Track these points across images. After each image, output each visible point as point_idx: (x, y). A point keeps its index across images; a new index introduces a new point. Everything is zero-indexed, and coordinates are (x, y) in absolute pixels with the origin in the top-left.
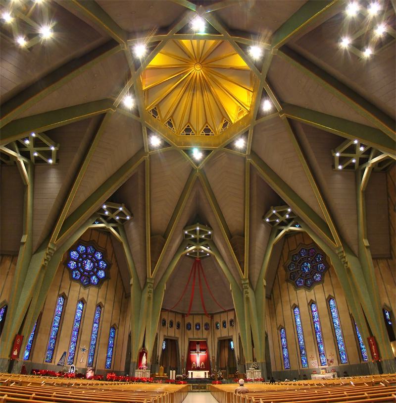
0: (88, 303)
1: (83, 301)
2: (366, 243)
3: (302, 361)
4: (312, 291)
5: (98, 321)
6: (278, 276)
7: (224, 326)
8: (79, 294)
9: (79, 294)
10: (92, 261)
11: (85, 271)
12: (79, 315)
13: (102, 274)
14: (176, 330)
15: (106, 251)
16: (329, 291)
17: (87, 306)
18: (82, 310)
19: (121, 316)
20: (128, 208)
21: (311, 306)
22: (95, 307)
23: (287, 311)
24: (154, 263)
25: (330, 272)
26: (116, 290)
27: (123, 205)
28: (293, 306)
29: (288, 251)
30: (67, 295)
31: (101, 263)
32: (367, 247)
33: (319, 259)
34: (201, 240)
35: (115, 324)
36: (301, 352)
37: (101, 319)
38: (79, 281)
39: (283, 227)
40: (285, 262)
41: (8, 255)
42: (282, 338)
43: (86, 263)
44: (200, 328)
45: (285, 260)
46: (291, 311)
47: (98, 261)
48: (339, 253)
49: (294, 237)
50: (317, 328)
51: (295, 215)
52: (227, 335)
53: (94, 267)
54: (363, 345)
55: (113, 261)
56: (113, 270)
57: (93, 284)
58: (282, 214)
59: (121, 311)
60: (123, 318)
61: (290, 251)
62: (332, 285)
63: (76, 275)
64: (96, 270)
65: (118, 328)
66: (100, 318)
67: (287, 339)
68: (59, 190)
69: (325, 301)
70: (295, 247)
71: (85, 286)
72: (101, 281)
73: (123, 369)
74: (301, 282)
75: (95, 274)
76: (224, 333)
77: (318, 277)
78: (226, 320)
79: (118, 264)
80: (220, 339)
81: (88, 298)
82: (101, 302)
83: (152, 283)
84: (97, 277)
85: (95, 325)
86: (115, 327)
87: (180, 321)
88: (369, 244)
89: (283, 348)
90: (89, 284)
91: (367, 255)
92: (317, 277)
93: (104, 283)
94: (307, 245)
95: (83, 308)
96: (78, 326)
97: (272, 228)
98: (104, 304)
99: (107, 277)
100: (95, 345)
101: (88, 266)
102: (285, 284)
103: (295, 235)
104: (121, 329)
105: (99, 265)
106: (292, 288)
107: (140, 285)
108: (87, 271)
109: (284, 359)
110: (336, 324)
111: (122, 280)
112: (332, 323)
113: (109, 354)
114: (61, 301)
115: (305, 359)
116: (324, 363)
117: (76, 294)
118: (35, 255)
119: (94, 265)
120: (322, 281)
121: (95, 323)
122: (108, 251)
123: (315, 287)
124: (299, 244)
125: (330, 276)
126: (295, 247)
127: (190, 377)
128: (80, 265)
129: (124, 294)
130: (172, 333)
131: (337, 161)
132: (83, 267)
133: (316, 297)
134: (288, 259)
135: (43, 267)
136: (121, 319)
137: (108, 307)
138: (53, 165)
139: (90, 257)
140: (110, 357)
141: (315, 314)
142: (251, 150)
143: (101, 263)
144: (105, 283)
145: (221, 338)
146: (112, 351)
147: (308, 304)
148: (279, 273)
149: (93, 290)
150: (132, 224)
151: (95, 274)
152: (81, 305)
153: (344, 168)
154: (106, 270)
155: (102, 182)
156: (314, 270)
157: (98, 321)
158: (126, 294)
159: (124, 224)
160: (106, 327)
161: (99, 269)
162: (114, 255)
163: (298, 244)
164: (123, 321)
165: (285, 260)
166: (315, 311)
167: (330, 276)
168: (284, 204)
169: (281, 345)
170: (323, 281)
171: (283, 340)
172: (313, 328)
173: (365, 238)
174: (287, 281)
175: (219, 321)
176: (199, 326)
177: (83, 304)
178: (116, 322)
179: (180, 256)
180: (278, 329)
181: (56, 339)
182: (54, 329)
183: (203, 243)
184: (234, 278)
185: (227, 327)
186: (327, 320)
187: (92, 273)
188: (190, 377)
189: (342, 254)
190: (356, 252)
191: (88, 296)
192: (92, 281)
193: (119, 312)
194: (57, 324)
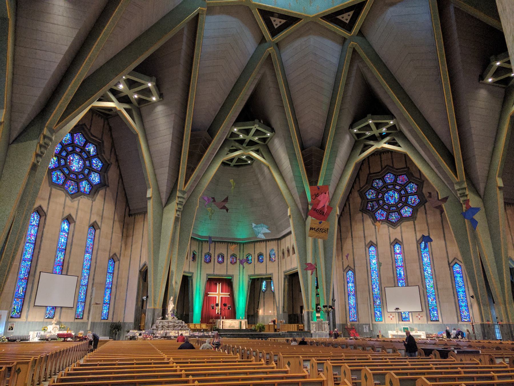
0: (76, 223)
1: (69, 219)
2: (500, 183)
3: (375, 313)
4: (399, 228)
5: (91, 250)
6: (349, 204)
7: (260, 261)
8: (64, 208)
9: (64, 208)
10: (82, 158)
11: (71, 172)
12: (63, 240)
13: (95, 178)
14: (191, 262)
15: (103, 142)
16: (422, 230)
17: (77, 226)
18: (68, 234)
19: (123, 242)
20: (158, 86)
21: (394, 246)
22: (88, 227)
23: (360, 247)
24: (190, 170)
25: (427, 207)
26: (116, 204)
27: (154, 78)
28: (368, 244)
29: (368, 172)
30: (45, 211)
31: (94, 162)
32: (500, 188)
33: (412, 189)
34: (251, 143)
35: (115, 254)
36: (374, 302)
37: (96, 246)
38: (62, 187)
39: (371, 143)
40: (361, 187)
41: (88, 181)
42: (348, 283)
43: (73, 160)
44: (223, 261)
45: (362, 184)
46: (366, 250)
47: (89, 158)
48: (459, 190)
49: (379, 156)
50: (400, 274)
51: (396, 129)
52: (265, 273)
53: (85, 167)
54: (463, 302)
55: (113, 160)
56: (113, 174)
57: (84, 194)
58: (378, 126)
59: (122, 235)
60: (126, 245)
61: (370, 174)
62: (428, 224)
63: (58, 178)
64: (86, 171)
65: (119, 260)
66: (93, 245)
67: (357, 283)
68: (71, 40)
69: (415, 242)
70: (379, 169)
71: (73, 196)
72: (94, 189)
73: (130, 318)
74: (382, 215)
75: (86, 178)
76: (260, 270)
77: (407, 212)
78: (264, 252)
79: (119, 166)
80: (252, 278)
81: (77, 214)
82: (95, 222)
83: (184, 198)
84: (90, 183)
85: (87, 256)
86: (115, 258)
87: (197, 251)
88: (504, 185)
89: (349, 295)
90: (78, 193)
91: (500, 198)
92: (406, 211)
93: (100, 192)
94: (397, 169)
95: (69, 230)
96: (62, 258)
97: (356, 141)
98: (99, 224)
99: (103, 184)
100: (87, 285)
101: (76, 164)
102: (360, 215)
103: (380, 155)
104: (124, 262)
105: (91, 163)
106: (369, 222)
107: (161, 199)
108: (73, 172)
109: (350, 308)
110: (427, 273)
111: (124, 189)
112: (422, 270)
113: (107, 298)
114: (34, 219)
115: (379, 311)
116: (406, 318)
117: (60, 208)
118: (14, 145)
119: (84, 164)
120: (413, 217)
121: (87, 252)
122: (105, 144)
123: (402, 224)
124: (385, 167)
125: (426, 213)
126: (379, 169)
127: (221, 328)
128: (62, 162)
129: (127, 210)
130: (188, 267)
131: (493, 70)
132: (67, 166)
133: (403, 236)
134: (367, 183)
135: (177, 219)
136: (123, 246)
137: (106, 228)
138: (489, 84)
139: (78, 150)
140: (107, 303)
141: (399, 257)
142: (360, 31)
143: (94, 162)
144: (102, 192)
145: (254, 275)
146: (110, 294)
147: (391, 244)
148: (351, 199)
149: (84, 202)
150: (160, 109)
151: (86, 178)
152: (65, 226)
153: (496, 82)
154: (103, 172)
155: (133, 39)
156: (403, 202)
157: (91, 250)
158: (130, 210)
159: (267, 142)
160: (103, 257)
161: (91, 170)
162: (113, 150)
163: (383, 167)
164: (126, 249)
165: (362, 184)
166: (398, 254)
167: (426, 213)
168: (387, 113)
169: (346, 291)
170: (416, 218)
171: (350, 285)
172: (395, 275)
173: (499, 176)
174: (360, 211)
175: (252, 253)
176: (223, 257)
177: (69, 224)
178: (116, 250)
179: (220, 163)
180: (344, 271)
181: (27, 279)
182: (23, 264)
183: (254, 148)
184: (294, 201)
185: (264, 261)
186: (416, 266)
187: (81, 176)
188: (221, 328)
189: (464, 191)
190: (482, 192)
191: (77, 211)
192: (82, 189)
193: (121, 236)
194: (28, 256)
